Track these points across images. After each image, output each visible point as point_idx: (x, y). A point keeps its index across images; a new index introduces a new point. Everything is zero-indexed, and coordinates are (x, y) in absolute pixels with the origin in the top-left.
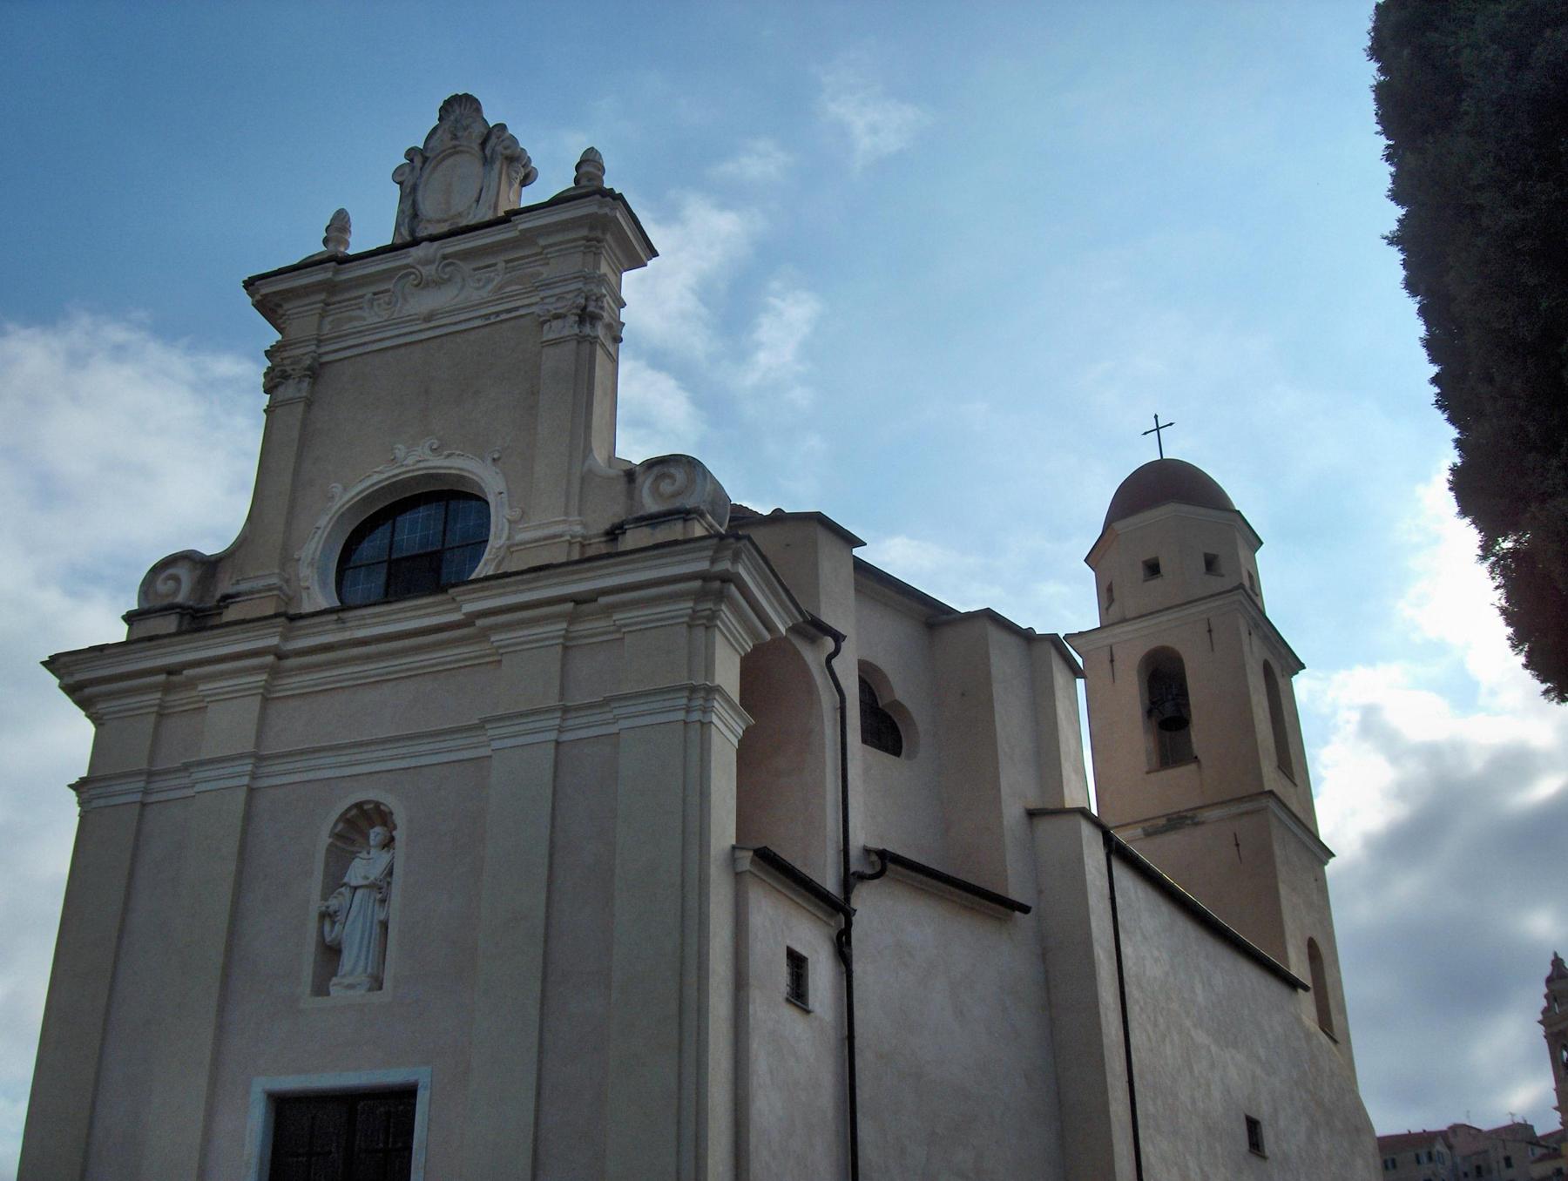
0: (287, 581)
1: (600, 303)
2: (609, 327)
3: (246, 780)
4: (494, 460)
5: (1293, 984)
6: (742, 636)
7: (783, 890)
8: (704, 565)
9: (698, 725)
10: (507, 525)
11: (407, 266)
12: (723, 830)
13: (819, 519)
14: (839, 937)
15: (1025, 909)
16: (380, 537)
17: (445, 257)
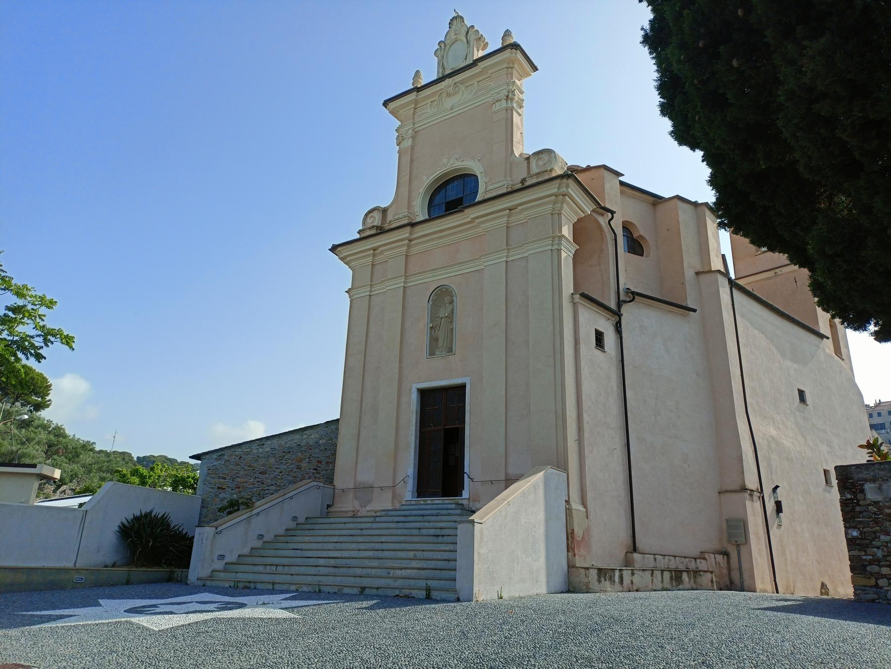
0: (411, 213)
3: (402, 284)
4: (478, 160)
5: (822, 336)
8: (555, 191)
9: (556, 250)
10: (484, 184)
11: (442, 89)
12: (568, 287)
15: (694, 311)
16: (442, 193)
17: (455, 84)
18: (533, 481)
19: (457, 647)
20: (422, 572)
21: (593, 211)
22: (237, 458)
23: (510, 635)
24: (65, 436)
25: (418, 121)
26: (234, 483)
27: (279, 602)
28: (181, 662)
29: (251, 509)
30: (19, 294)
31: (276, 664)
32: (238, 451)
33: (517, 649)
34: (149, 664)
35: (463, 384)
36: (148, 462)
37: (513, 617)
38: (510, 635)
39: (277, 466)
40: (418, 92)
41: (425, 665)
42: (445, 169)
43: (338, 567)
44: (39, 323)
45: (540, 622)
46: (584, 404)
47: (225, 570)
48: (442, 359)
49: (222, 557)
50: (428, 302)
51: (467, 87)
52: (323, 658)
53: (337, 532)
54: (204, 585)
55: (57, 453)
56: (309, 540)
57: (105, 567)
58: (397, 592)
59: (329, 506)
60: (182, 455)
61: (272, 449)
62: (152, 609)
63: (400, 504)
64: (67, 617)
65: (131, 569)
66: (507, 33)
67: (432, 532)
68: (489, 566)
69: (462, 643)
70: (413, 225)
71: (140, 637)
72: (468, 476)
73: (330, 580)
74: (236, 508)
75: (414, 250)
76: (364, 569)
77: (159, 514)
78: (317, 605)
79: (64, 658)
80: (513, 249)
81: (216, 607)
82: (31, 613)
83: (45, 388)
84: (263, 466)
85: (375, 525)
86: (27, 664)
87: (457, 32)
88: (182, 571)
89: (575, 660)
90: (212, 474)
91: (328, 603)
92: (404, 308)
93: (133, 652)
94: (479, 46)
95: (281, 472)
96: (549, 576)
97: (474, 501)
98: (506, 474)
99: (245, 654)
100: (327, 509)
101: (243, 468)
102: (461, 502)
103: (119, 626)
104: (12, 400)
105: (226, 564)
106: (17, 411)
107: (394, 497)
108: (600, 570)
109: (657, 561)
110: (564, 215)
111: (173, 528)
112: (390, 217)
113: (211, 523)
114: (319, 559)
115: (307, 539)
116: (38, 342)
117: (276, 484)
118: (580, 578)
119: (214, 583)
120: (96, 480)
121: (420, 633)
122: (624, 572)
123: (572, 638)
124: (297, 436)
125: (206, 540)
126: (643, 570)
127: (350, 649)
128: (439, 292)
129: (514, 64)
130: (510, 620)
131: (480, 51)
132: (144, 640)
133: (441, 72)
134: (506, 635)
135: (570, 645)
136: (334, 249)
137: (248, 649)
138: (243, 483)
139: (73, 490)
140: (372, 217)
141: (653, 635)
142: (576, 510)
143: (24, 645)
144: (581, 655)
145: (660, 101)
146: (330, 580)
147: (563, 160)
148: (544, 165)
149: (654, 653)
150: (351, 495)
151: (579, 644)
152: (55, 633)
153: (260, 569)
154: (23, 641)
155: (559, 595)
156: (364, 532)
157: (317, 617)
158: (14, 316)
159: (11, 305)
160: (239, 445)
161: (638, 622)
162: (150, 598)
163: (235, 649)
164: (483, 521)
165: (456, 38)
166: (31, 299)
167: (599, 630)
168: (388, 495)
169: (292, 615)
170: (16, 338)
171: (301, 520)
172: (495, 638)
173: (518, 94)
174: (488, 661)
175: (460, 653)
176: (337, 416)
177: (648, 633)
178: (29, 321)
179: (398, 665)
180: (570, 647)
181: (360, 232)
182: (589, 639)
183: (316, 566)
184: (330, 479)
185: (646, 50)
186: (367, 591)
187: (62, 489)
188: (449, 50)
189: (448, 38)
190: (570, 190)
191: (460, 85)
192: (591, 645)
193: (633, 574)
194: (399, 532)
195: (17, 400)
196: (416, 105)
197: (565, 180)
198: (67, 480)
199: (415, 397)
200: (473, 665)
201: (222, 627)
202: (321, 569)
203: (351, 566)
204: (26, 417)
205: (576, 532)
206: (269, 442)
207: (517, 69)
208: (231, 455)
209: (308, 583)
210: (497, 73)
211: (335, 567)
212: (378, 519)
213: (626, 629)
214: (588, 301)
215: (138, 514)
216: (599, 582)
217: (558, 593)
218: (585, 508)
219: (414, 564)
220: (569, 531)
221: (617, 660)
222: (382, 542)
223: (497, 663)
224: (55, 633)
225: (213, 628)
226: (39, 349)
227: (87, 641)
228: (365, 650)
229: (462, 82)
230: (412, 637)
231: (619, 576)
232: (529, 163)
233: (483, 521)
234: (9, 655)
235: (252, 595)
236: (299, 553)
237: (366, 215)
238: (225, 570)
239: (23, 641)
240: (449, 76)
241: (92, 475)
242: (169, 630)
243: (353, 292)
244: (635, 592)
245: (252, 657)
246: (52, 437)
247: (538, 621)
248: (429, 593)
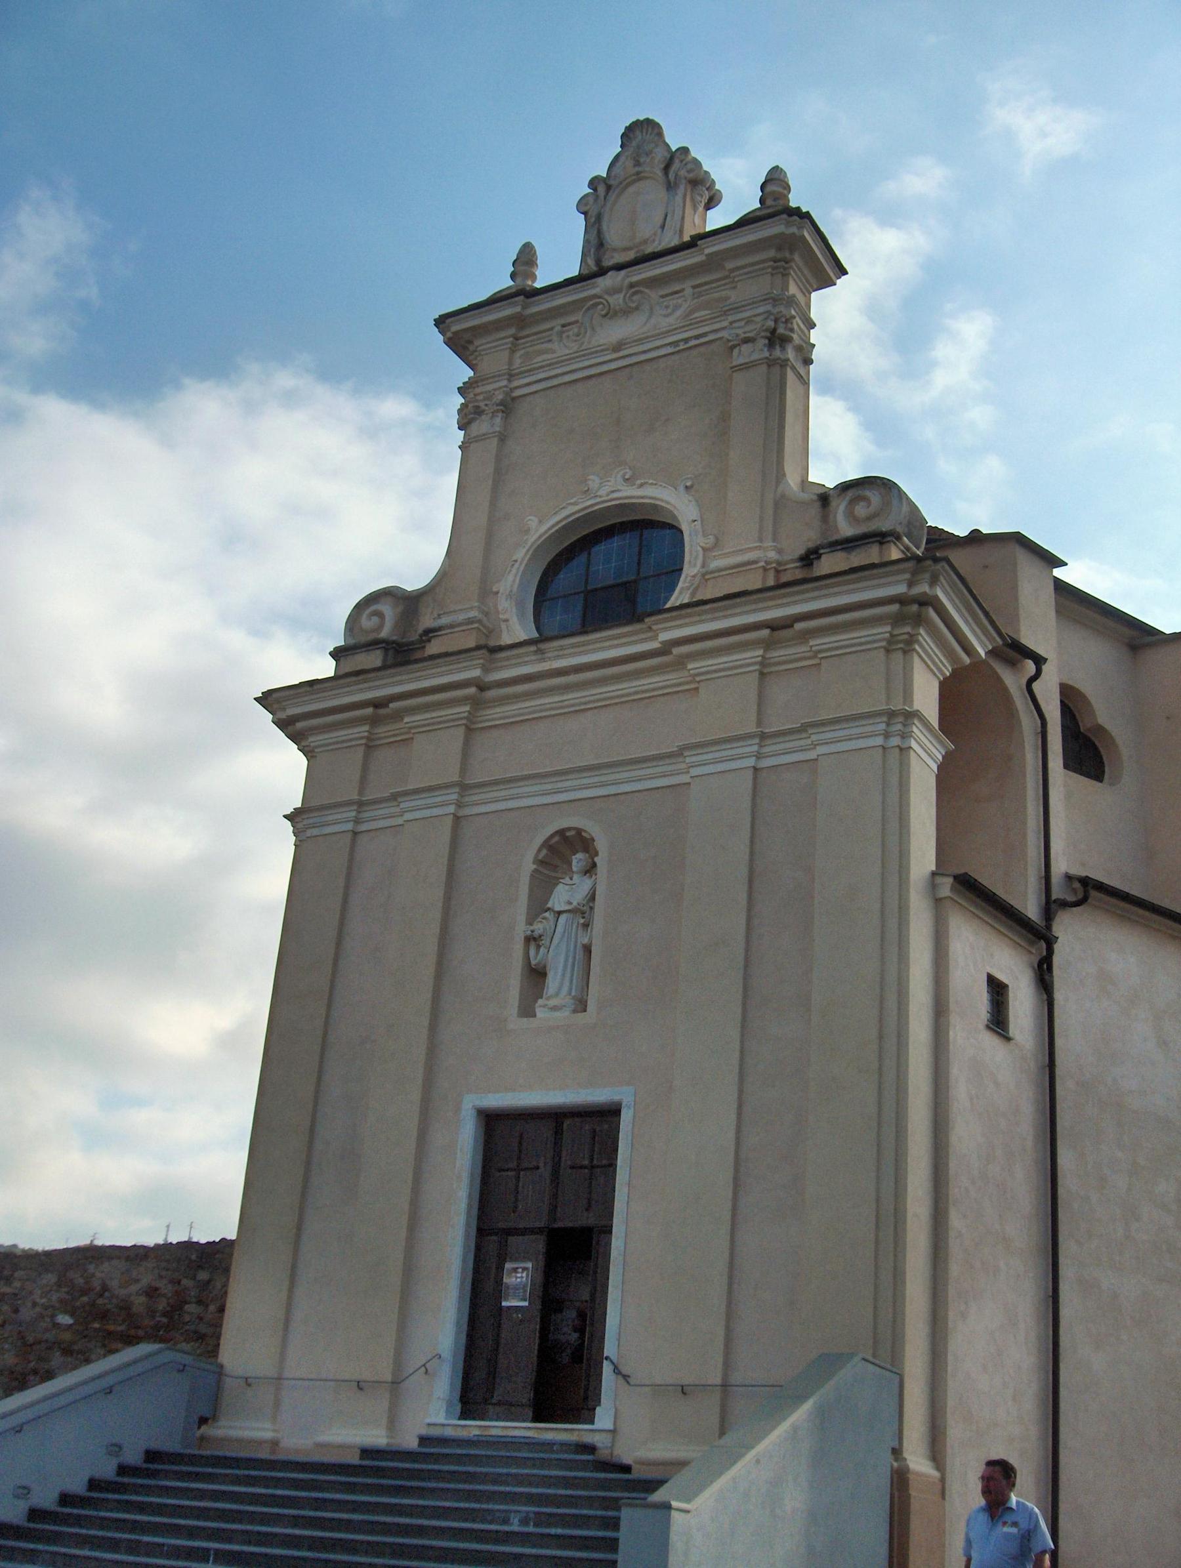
0: (487, 614)
1: (789, 325)
3: (452, 809)
11: (595, 296)
13: (1018, 539)
59: (203, 1421)
102: (588, 1439)
110: (920, 656)
214: (991, 909)
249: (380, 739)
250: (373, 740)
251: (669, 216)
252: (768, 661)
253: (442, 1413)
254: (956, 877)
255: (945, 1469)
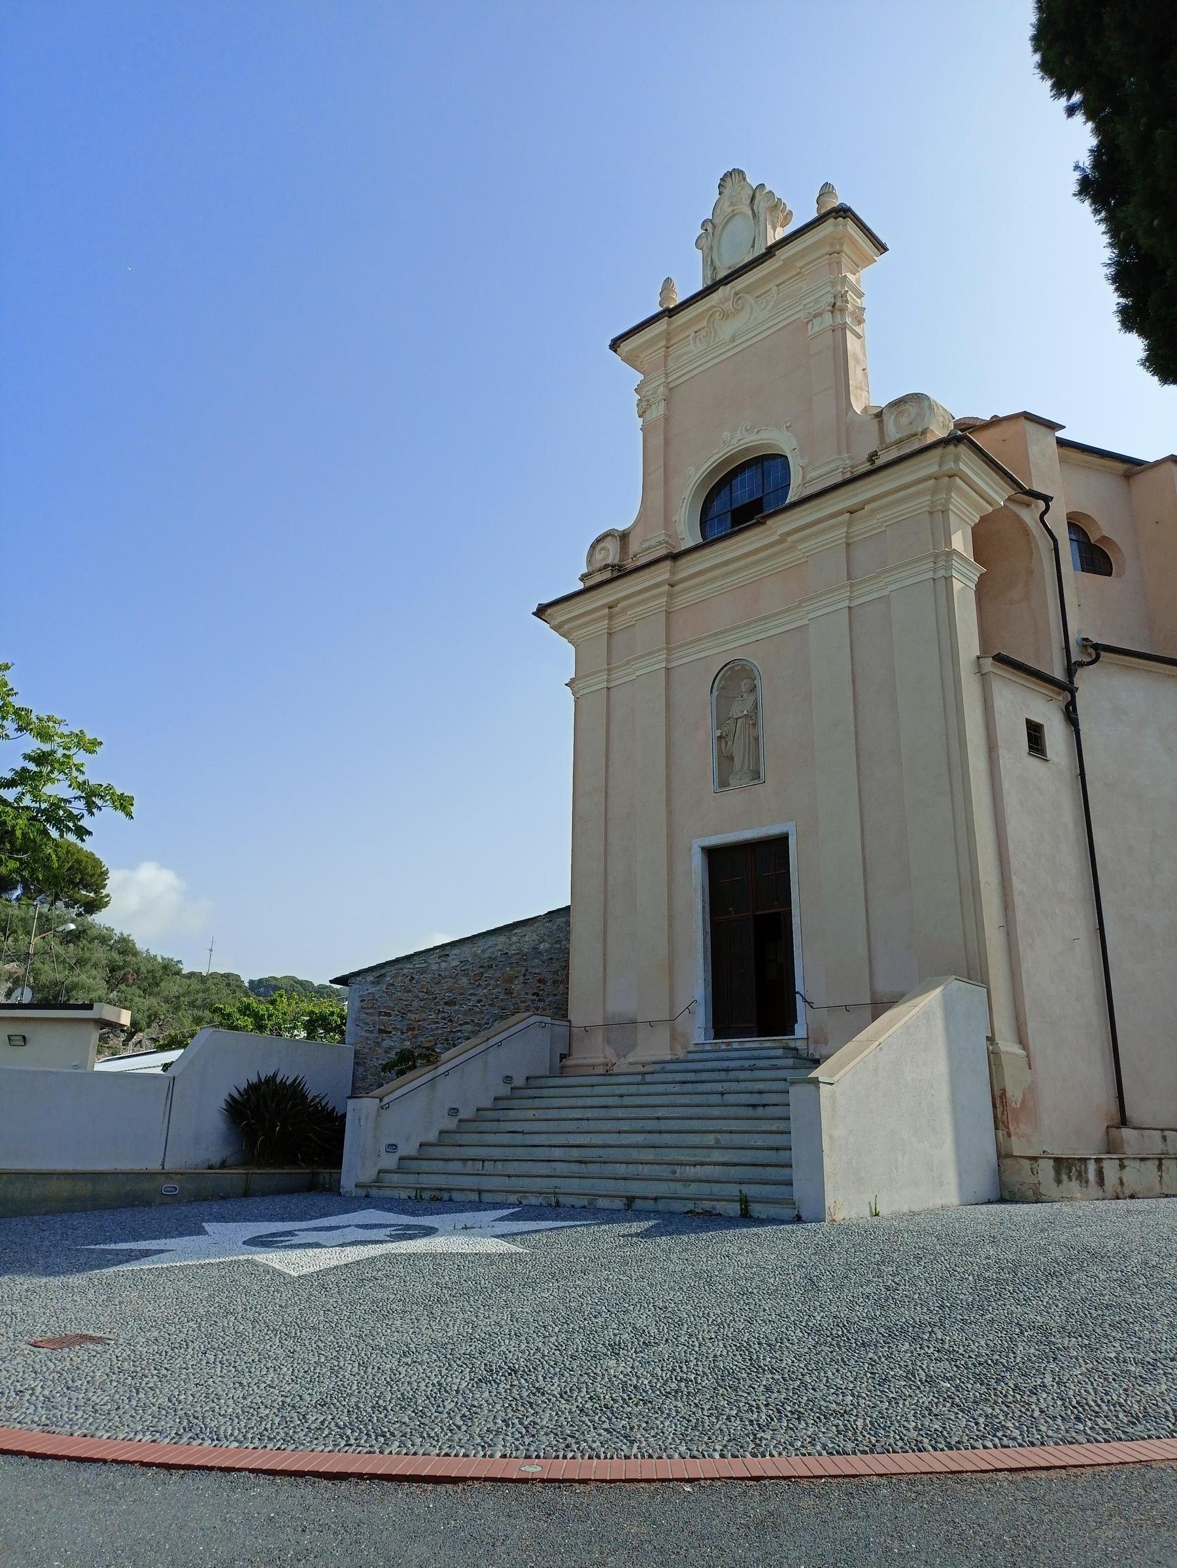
0: (670, 536)
1: (844, 298)
2: (853, 314)
6: (970, 513)
7: (1017, 680)
8: (934, 469)
11: (714, 307)
12: (969, 644)
13: (1028, 416)
14: (1067, 707)
16: (725, 495)
18: (921, 1005)
19: (800, 1306)
20: (733, 1169)
21: (1010, 499)
22: (407, 980)
23: (895, 1283)
24: (135, 954)
25: (674, 370)
26: (406, 1022)
27: (491, 1225)
28: (336, 1331)
29: (434, 1066)
30: (44, 735)
31: (490, 1335)
32: (408, 968)
33: (909, 1310)
34: (286, 1334)
35: (783, 834)
36: (264, 987)
37: (899, 1251)
38: (895, 1283)
39: (472, 991)
40: (670, 317)
41: (745, 1339)
42: (725, 452)
43: (585, 1163)
44: (76, 778)
45: (950, 1259)
46: (1012, 859)
47: (399, 1170)
48: (741, 791)
49: (392, 1148)
50: (711, 692)
51: (757, 297)
52: (568, 1325)
53: (580, 1102)
54: (367, 1196)
55: (124, 980)
56: (534, 1115)
57: (211, 1167)
58: (690, 1206)
59: (563, 1057)
60: (321, 978)
61: (461, 962)
62: (286, 1238)
63: (685, 1050)
64: (155, 1254)
65: (251, 1171)
66: (827, 190)
67: (744, 1099)
68: (850, 1159)
69: (810, 1299)
70: (675, 557)
71: (270, 1287)
72: (803, 998)
73: (574, 1185)
74: (410, 1063)
75: (681, 601)
76: (630, 1166)
77: (288, 1078)
78: (554, 1229)
79: (154, 1323)
80: (860, 583)
81: (388, 1233)
82: (102, 1247)
83: (99, 876)
84: (450, 992)
85: (644, 1089)
86: (99, 1335)
87: (734, 201)
88: (330, 1173)
89: (1017, 1331)
90: (369, 1008)
91: (572, 1226)
92: (668, 706)
93: (259, 1314)
94: (776, 220)
95: (480, 1001)
96: (961, 1174)
97: (817, 1042)
98: (873, 993)
99: (439, 1318)
100: (561, 1061)
101: (417, 997)
102: (792, 1044)
103: (235, 1269)
104: (50, 899)
105: (401, 1159)
106: (59, 917)
107: (673, 1038)
108: (1058, 1161)
109: (1168, 1142)
110: (954, 512)
111: (312, 1100)
112: (634, 546)
113: (372, 1090)
114: (553, 1148)
115: (530, 1114)
116: (78, 807)
117: (473, 1021)
118: (1022, 1175)
119: (387, 1193)
120: (187, 1022)
121: (734, 1281)
122: (1105, 1164)
123: (1011, 1289)
124: (501, 939)
125: (367, 1119)
126: (1142, 1159)
127: (612, 1310)
128: (729, 673)
129: (842, 245)
130: (895, 1255)
131: (779, 229)
132: (276, 1293)
133: (709, 276)
134: (889, 1284)
135: (1007, 1303)
136: (541, 612)
137: (442, 1309)
138: (419, 1021)
139: (154, 1040)
140: (603, 549)
141: (1166, 1284)
142: (1009, 1053)
143: (94, 1302)
144: (1029, 1322)
145: (1118, 304)
146: (574, 1185)
147: (945, 410)
148: (911, 423)
149: (1170, 1319)
150: (600, 1038)
151: (1025, 1300)
152: (140, 1281)
153: (456, 1166)
154: (91, 1295)
155: (984, 1208)
156: (627, 1101)
157: (555, 1251)
158: (36, 769)
159: (33, 751)
160: (408, 958)
161: (1135, 1259)
162: (282, 1220)
163: (422, 1308)
164: (835, 1079)
165: (733, 211)
166: (62, 740)
167: (1062, 1275)
168: (663, 1035)
169: (514, 1248)
170: (44, 806)
171: (519, 1081)
172: (868, 1290)
173: (854, 299)
174: (857, 1332)
175: (806, 1318)
176: (565, 901)
177: (1156, 1280)
178: (62, 776)
179: (697, 1338)
180: (1008, 1306)
181: (583, 578)
182: (1044, 1291)
183: (549, 1161)
184: (561, 1010)
185: (1086, 207)
186: (638, 1204)
187: (136, 1038)
188: (721, 236)
189: (719, 211)
190: (962, 466)
191: (745, 295)
192: (1047, 1302)
193: (1122, 1167)
194: (686, 1100)
195: (57, 898)
196: (668, 340)
197: (951, 448)
198: (144, 1024)
199: (697, 863)
200: (829, 1339)
201: (399, 1269)
202: (557, 1165)
203: (608, 1160)
204: (72, 926)
205: (1009, 1094)
206: (456, 951)
207: (849, 253)
208: (395, 976)
209: (538, 1190)
210: (811, 265)
211: (580, 1162)
212: (648, 1078)
213: (1114, 1272)
215: (255, 1080)
216: (1059, 1181)
217: (981, 1204)
218: (1024, 1049)
219: (716, 1156)
220: (997, 1093)
221: (1097, 1331)
222: (658, 1118)
223: (874, 1336)
224: (140, 1281)
225: (384, 1272)
226: (79, 820)
227: (188, 1295)
228: (639, 1311)
229: (749, 289)
230: (720, 1287)
231: (1095, 1170)
232: (881, 422)
233: (835, 1079)
234: (71, 1320)
235: (446, 1213)
236: (518, 1139)
237: (593, 547)
238: (399, 1170)
239: (91, 1295)
240: (726, 281)
241: (180, 1014)
242: (315, 1275)
243: (579, 684)
244: (1128, 1200)
245: (451, 1323)
246: (115, 955)
247: (947, 1258)
248: (746, 1207)
249: (614, 628)
250: (612, 629)
251: (756, 239)
252: (851, 535)
253: (703, 1037)
254: (994, 658)
255: (1028, 1048)
